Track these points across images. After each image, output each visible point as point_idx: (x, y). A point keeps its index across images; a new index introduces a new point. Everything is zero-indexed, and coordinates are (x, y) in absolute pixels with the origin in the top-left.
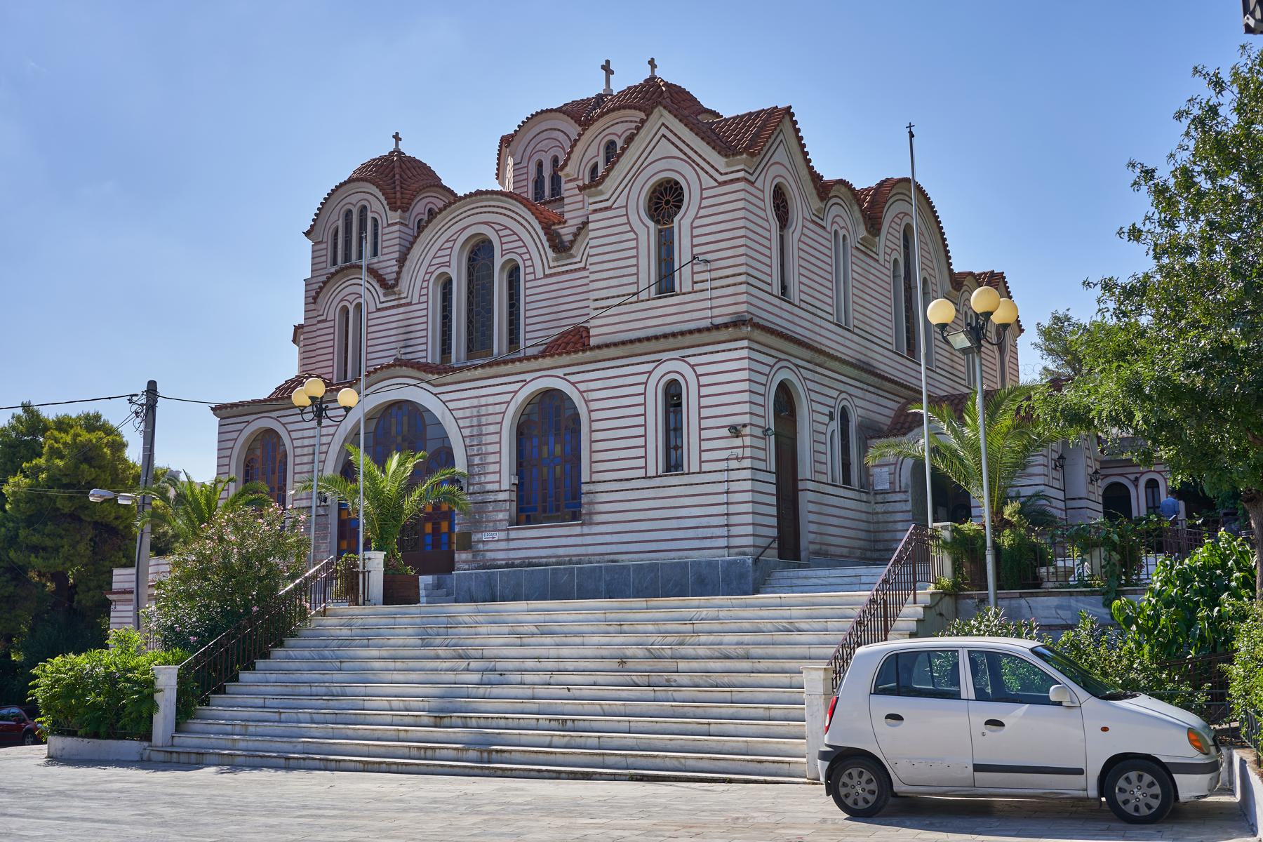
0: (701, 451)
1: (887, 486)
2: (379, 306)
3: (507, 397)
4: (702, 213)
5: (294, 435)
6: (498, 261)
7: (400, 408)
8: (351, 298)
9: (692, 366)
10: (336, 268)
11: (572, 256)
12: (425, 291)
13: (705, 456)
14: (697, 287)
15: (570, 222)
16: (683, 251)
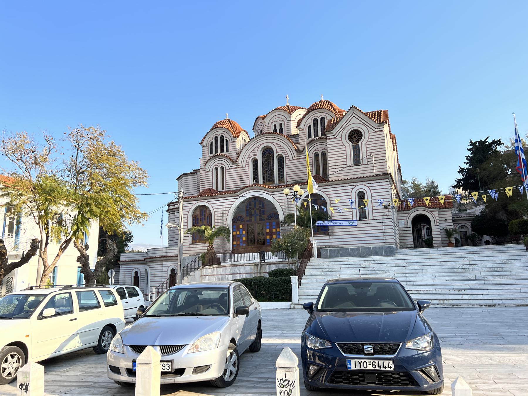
0: (373, 213)
1: (403, 226)
3: (189, 207)
6: (275, 155)
8: (219, 165)
10: (212, 155)
13: (374, 215)
14: (369, 163)
15: (301, 143)
16: (363, 154)
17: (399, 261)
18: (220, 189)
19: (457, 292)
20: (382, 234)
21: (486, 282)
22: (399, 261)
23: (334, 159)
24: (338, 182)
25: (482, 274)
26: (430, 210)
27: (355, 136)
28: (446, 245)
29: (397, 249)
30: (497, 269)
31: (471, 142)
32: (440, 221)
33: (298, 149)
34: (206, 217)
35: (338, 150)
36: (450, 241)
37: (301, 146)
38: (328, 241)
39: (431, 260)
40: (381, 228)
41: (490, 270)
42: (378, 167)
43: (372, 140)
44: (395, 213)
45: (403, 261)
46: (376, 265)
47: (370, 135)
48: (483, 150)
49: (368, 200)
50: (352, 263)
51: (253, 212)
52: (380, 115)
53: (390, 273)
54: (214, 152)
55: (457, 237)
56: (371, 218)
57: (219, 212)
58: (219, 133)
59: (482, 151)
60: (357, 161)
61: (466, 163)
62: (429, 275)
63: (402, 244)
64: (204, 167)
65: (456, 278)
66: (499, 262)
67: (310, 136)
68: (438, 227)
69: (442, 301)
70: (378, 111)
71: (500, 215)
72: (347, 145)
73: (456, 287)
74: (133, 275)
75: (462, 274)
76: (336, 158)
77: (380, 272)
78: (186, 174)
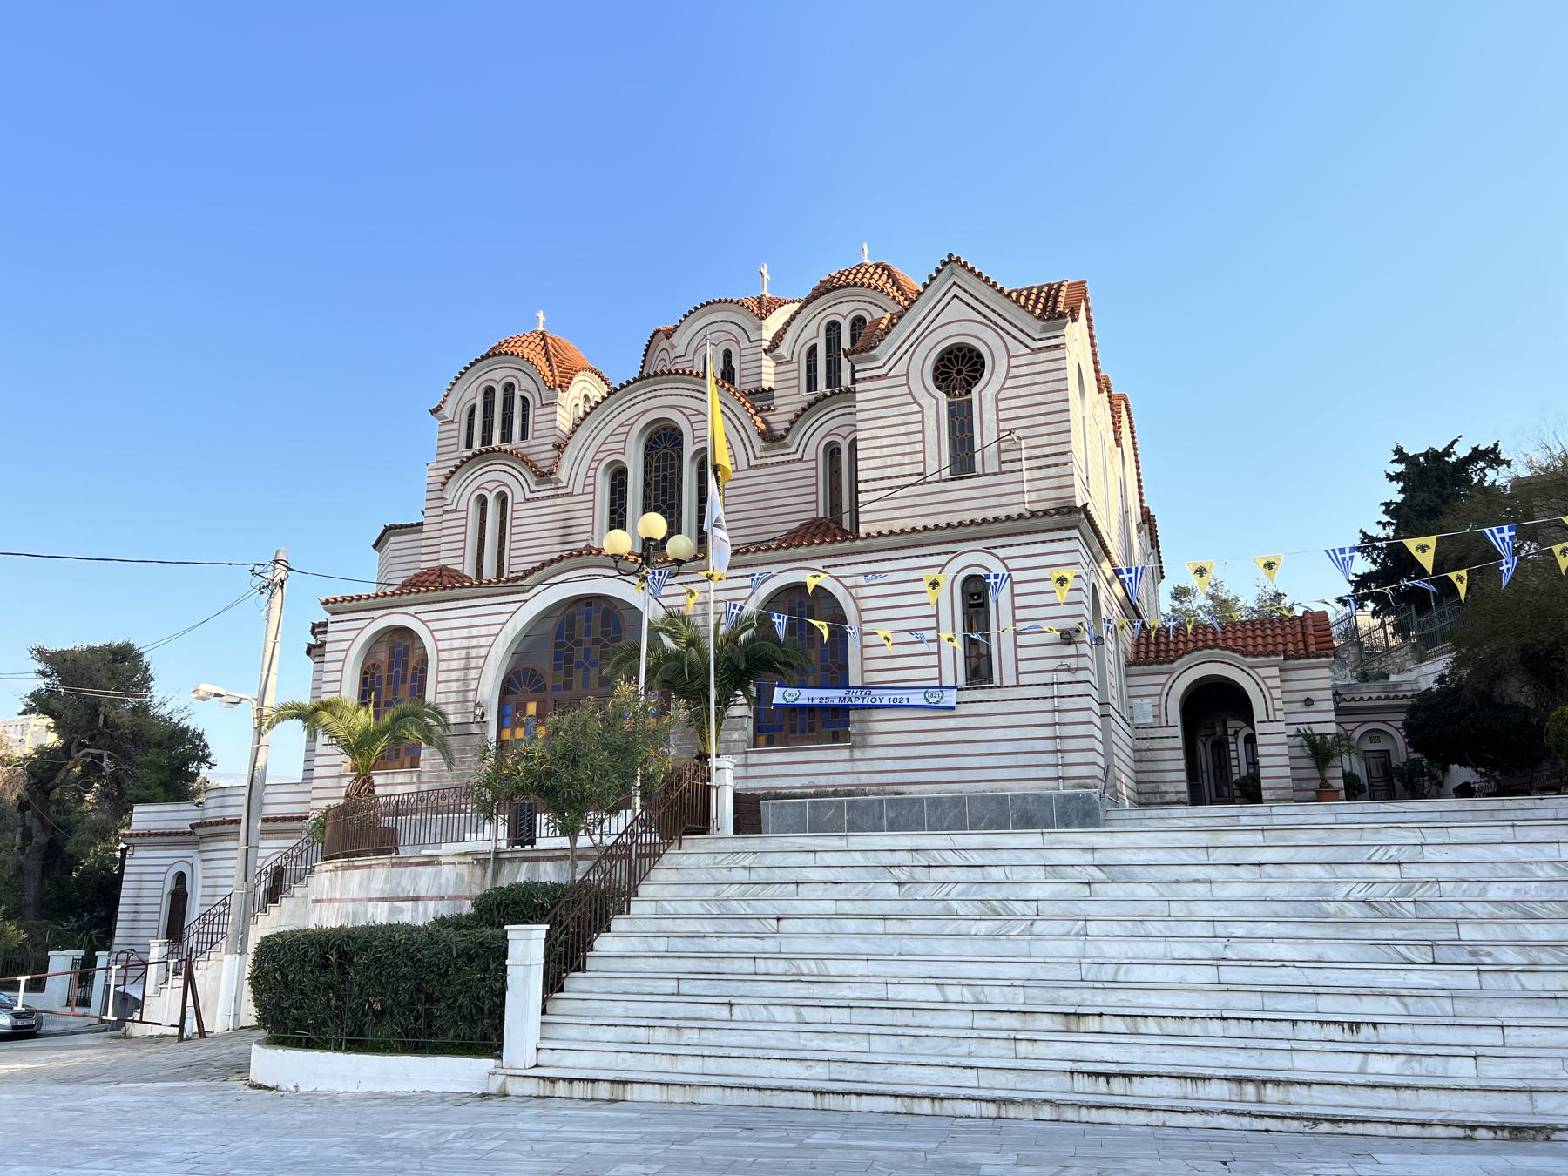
0: (1017, 660)
1: (1150, 720)
2: (529, 496)
3: (352, 635)
4: (1010, 383)
5: (438, 635)
6: (688, 450)
7: (589, 605)
8: (490, 486)
9: (1002, 560)
10: (469, 453)
11: (786, 446)
12: (590, 481)
13: (1023, 666)
14: (1005, 467)
16: (985, 429)
17: (1066, 857)
18: (489, 572)
19: (1334, 1032)
20: (1048, 745)
21: (1491, 981)
22: (1066, 857)
23: (877, 453)
24: (891, 539)
25: (1467, 932)
26: (1249, 660)
27: (959, 368)
29: (1116, 802)
30: (1540, 911)
31: (1399, 451)
32: (1286, 706)
33: (770, 430)
34: (410, 672)
35: (896, 424)
36: (1323, 780)
37: (779, 420)
38: (847, 767)
39: (1217, 856)
40: (1047, 718)
41: (1505, 912)
42: (1039, 484)
43: (1022, 381)
45: (1088, 857)
46: (960, 874)
47: (1014, 362)
48: (1439, 479)
49: (1000, 603)
50: (859, 859)
51: (578, 653)
52: (1056, 297)
53: (1012, 916)
54: (477, 444)
55: (1356, 771)
56: (1009, 679)
57: (455, 654)
58: (498, 375)
59: (1435, 487)
60: (963, 460)
61: (1385, 525)
62: (1197, 929)
64: (438, 494)
65: (1331, 952)
66: (1548, 872)
67: (811, 384)
68: (1281, 727)
69: (1250, 1090)
70: (1050, 286)
71: (1511, 690)
72: (926, 401)
73: (1330, 1006)
74: (169, 886)
75: (1365, 932)
76: (886, 451)
77: (971, 908)
78: (401, 526)
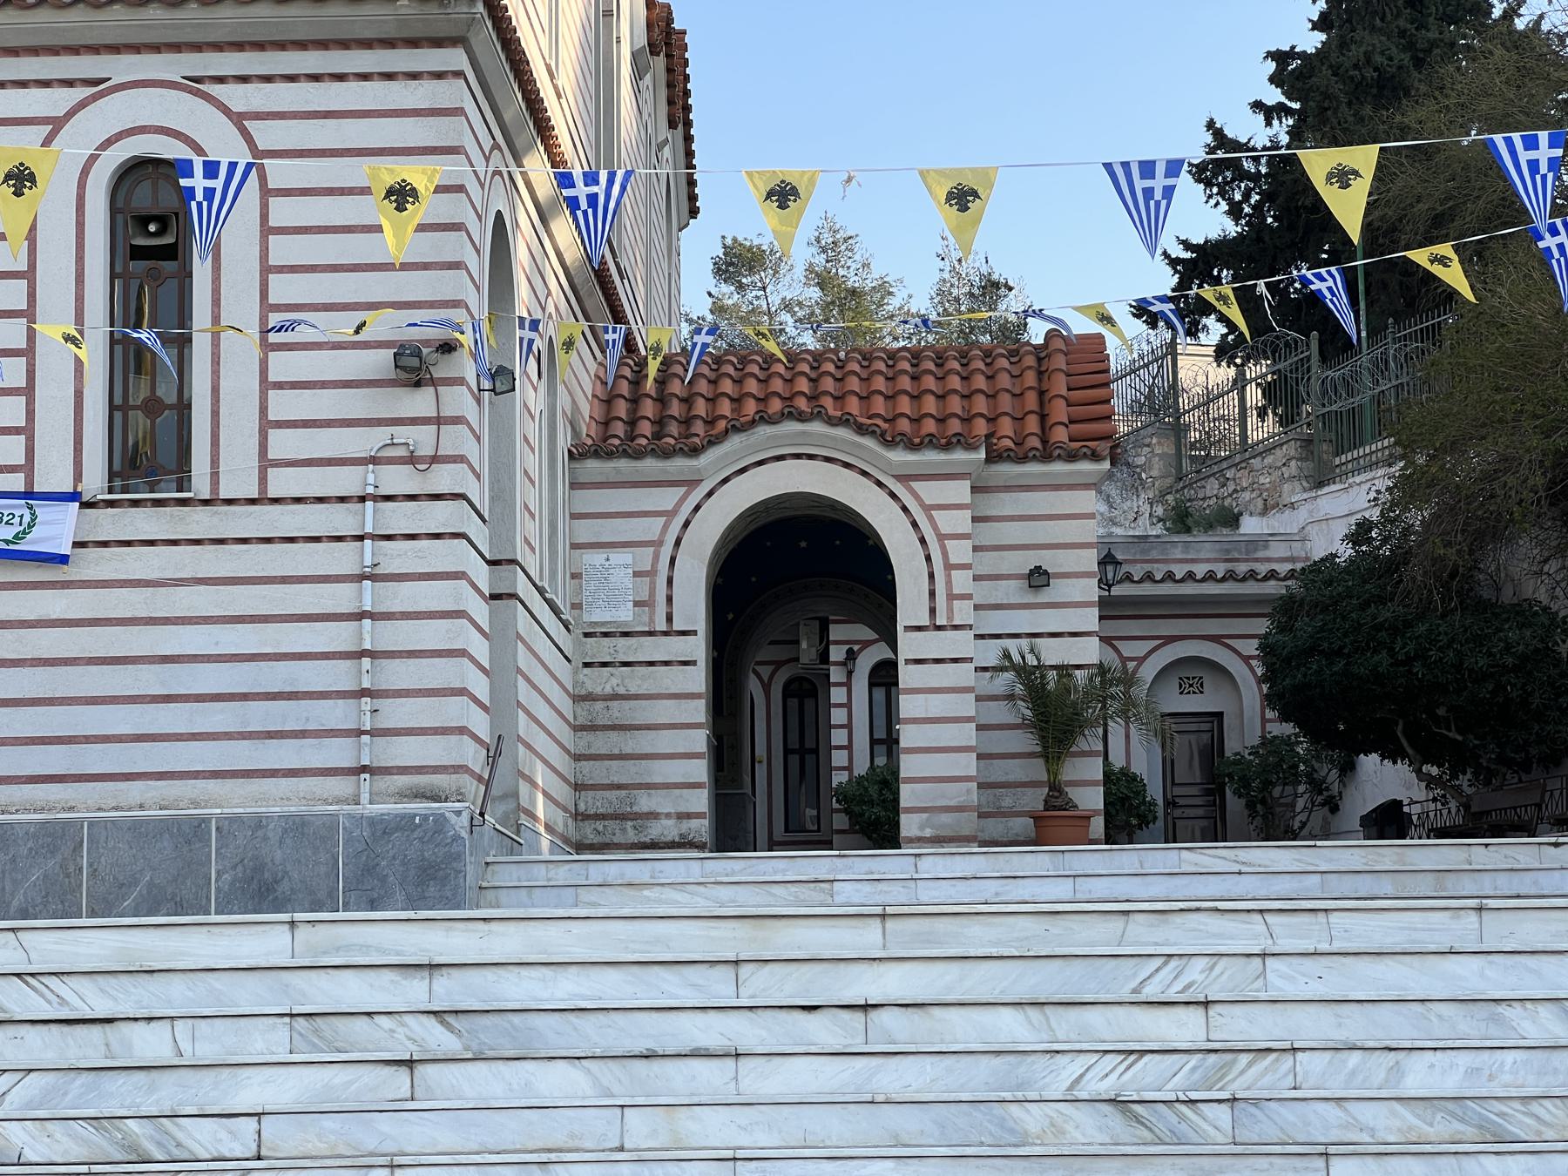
0: (266, 425)
1: (625, 615)
13: (283, 444)
20: (338, 675)
26: (899, 456)
28: (1023, 825)
29: (513, 840)
32: (984, 578)
39: (762, 985)
40: (340, 598)
41: (1440, 1127)
44: (531, 461)
45: (415, 991)
49: (227, 275)
55: (1139, 767)
56: (239, 480)
63: (593, 802)
68: (960, 643)
